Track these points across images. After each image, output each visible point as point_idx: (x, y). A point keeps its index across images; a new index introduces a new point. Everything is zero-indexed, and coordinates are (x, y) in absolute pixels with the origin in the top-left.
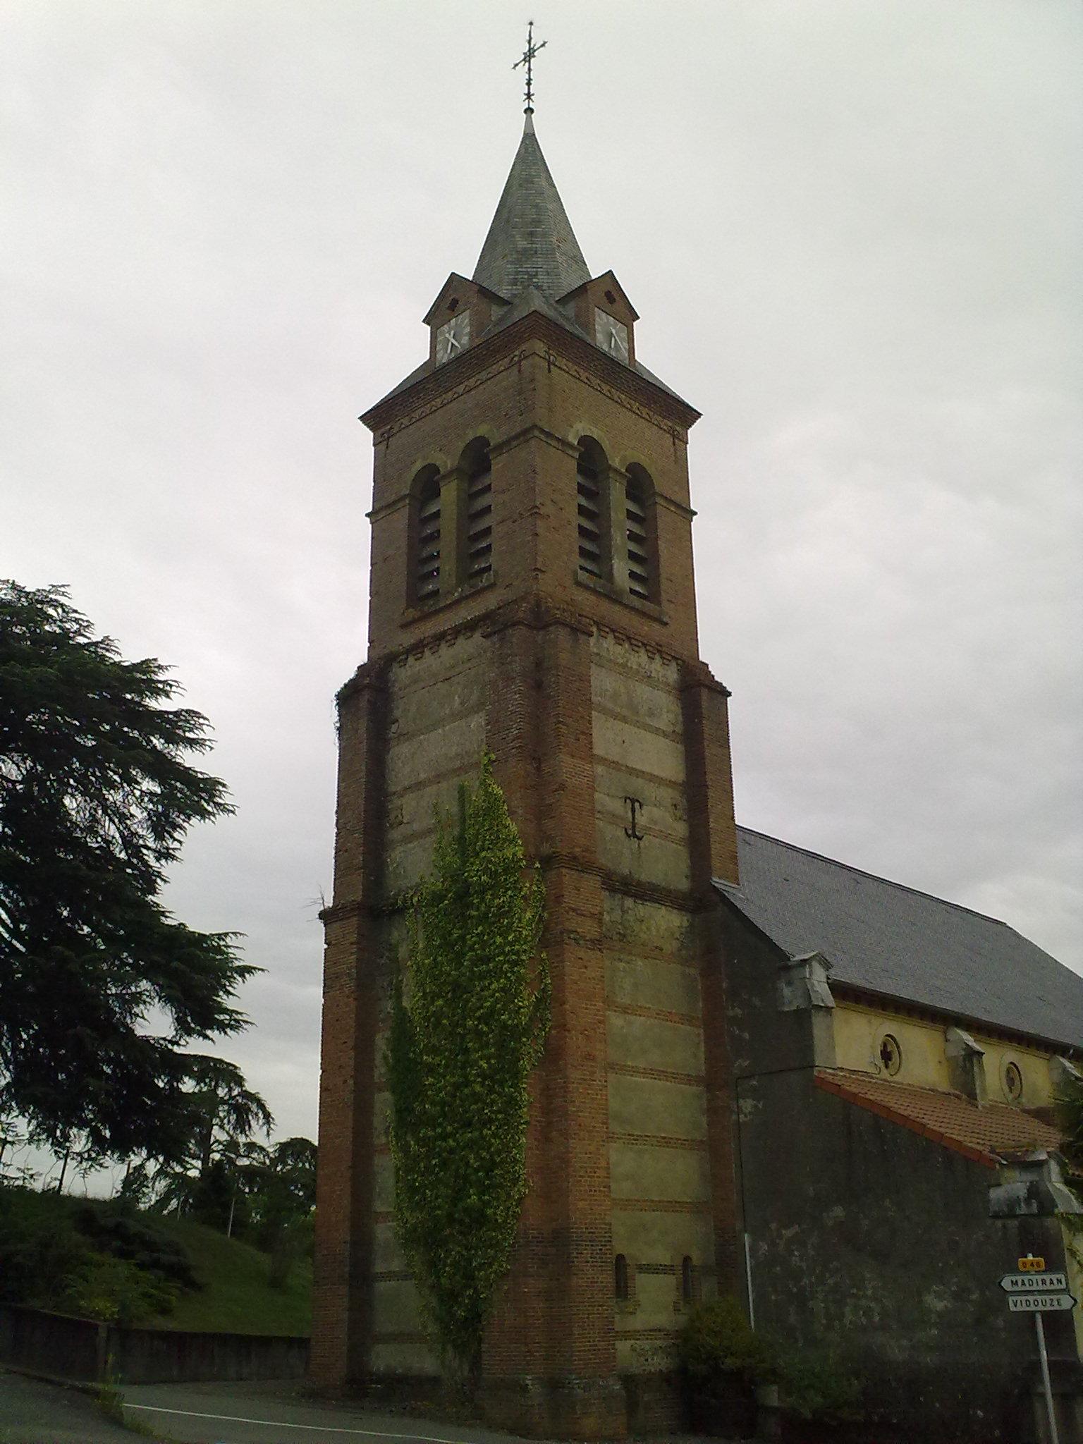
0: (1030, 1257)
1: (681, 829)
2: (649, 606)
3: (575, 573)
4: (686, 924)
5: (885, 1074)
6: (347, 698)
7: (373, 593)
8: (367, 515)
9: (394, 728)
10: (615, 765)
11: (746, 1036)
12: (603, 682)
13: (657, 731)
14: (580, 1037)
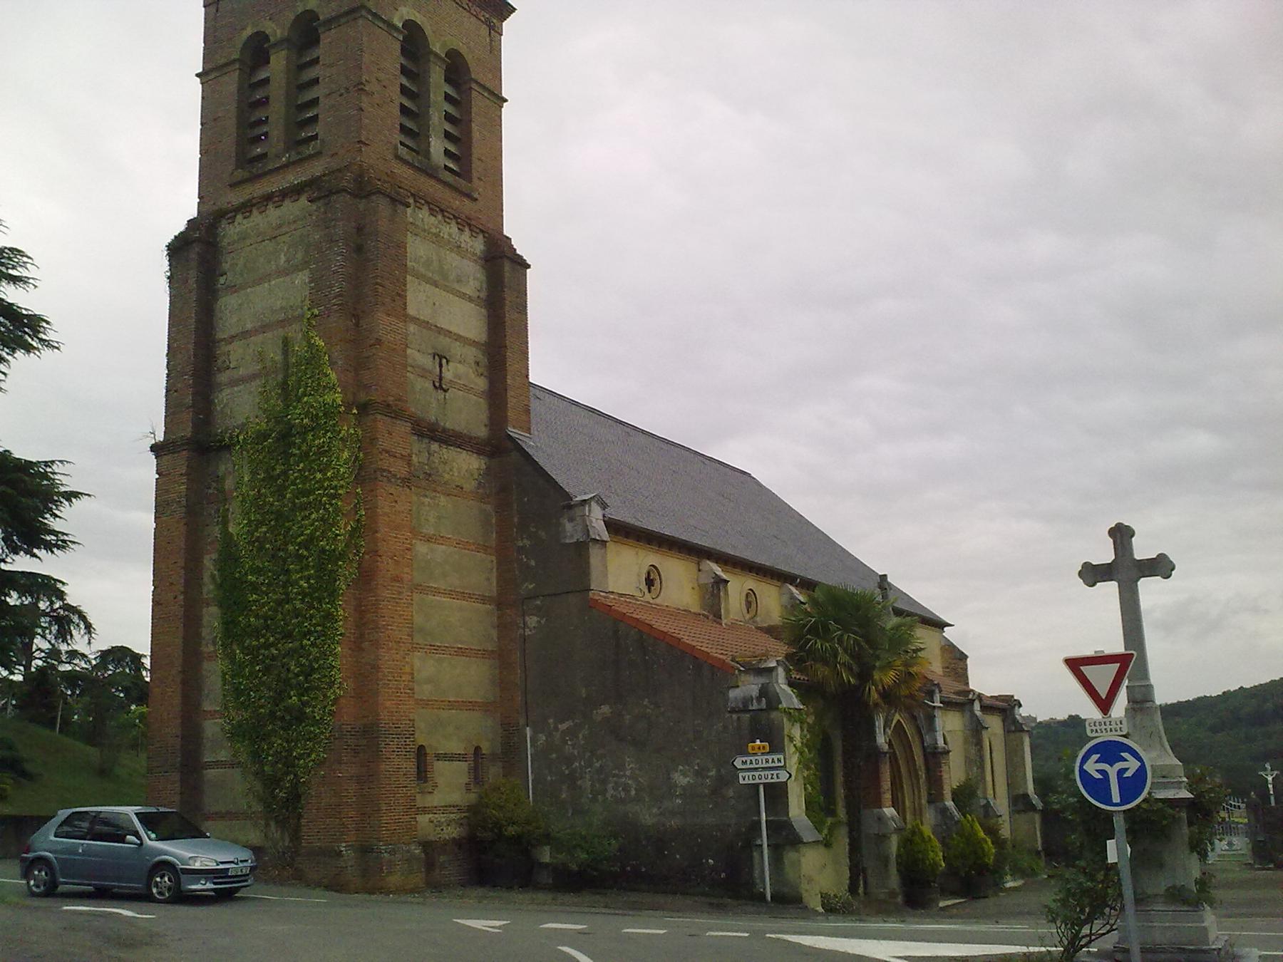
0: (758, 742)
1: (482, 384)
2: (461, 183)
3: (396, 148)
4: (484, 466)
5: (648, 597)
6: (177, 249)
8: (197, 75)
10: (426, 325)
11: (533, 563)
12: (417, 249)
13: (462, 296)
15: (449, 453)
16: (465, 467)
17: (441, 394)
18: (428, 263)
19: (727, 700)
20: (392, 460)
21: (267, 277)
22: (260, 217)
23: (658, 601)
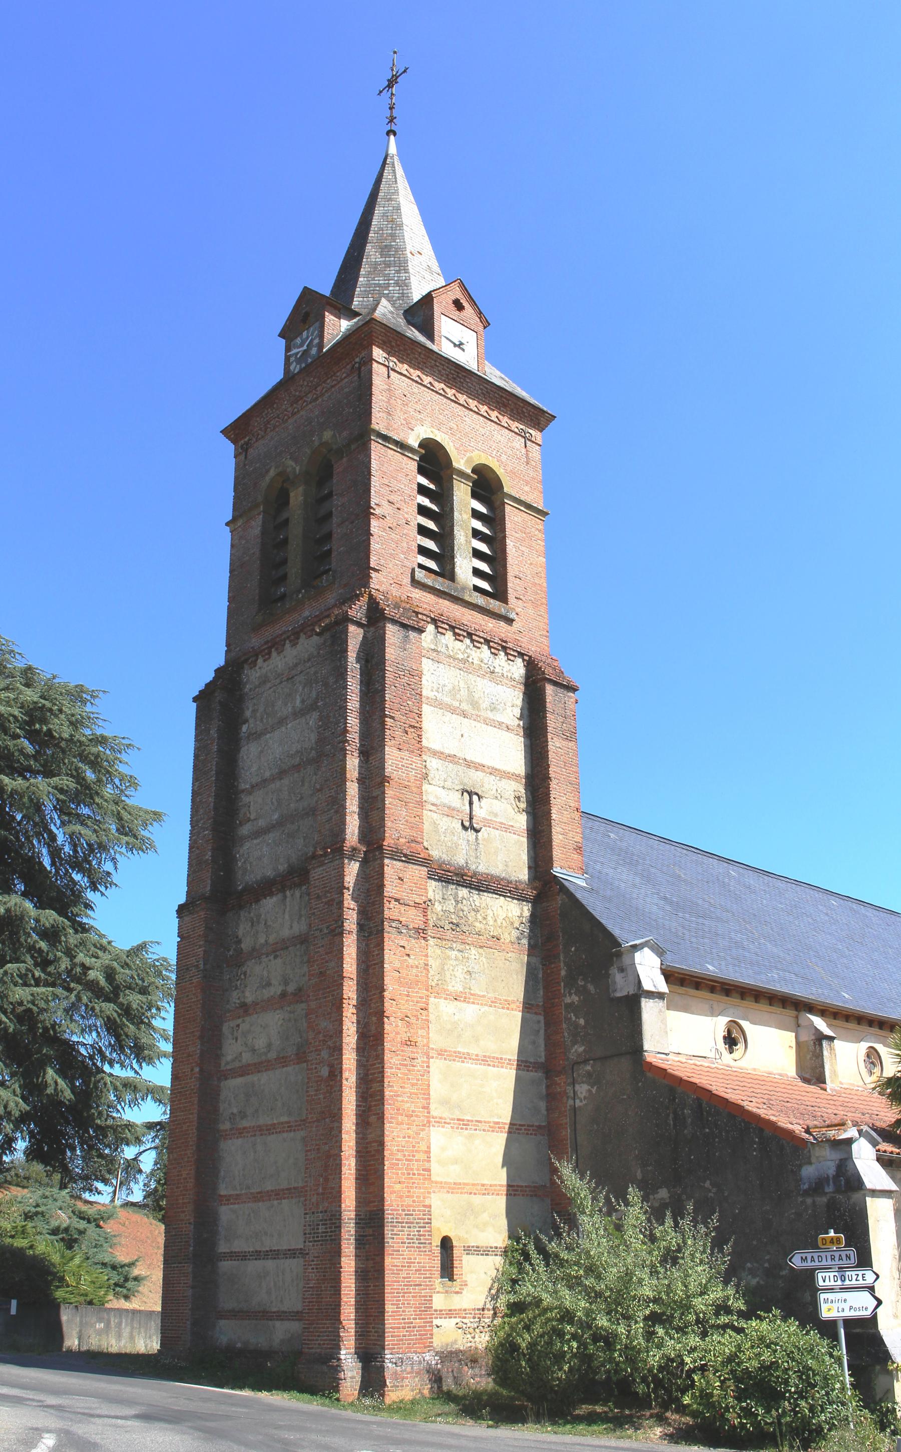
0: (832, 1233)
1: (522, 821)
2: (494, 605)
3: (413, 570)
4: (527, 914)
5: (727, 1058)
6: (203, 699)
7: (231, 599)
8: (227, 524)
9: (244, 728)
10: (451, 758)
11: (582, 1022)
12: (435, 678)
13: (500, 725)
14: (400, 1023)
15: (487, 899)
16: (502, 914)
17: (471, 834)
18: (454, 692)
19: (799, 1180)
20: (403, 908)
21: (282, 722)
22: (278, 658)
23: (738, 1064)
